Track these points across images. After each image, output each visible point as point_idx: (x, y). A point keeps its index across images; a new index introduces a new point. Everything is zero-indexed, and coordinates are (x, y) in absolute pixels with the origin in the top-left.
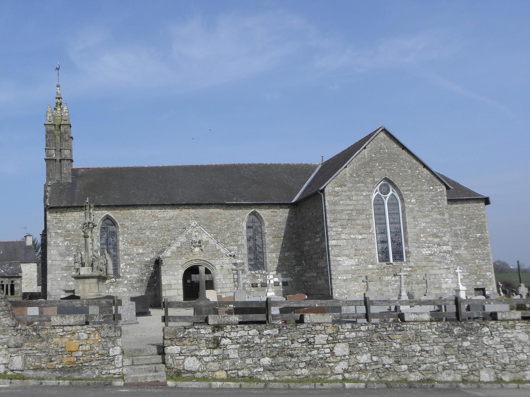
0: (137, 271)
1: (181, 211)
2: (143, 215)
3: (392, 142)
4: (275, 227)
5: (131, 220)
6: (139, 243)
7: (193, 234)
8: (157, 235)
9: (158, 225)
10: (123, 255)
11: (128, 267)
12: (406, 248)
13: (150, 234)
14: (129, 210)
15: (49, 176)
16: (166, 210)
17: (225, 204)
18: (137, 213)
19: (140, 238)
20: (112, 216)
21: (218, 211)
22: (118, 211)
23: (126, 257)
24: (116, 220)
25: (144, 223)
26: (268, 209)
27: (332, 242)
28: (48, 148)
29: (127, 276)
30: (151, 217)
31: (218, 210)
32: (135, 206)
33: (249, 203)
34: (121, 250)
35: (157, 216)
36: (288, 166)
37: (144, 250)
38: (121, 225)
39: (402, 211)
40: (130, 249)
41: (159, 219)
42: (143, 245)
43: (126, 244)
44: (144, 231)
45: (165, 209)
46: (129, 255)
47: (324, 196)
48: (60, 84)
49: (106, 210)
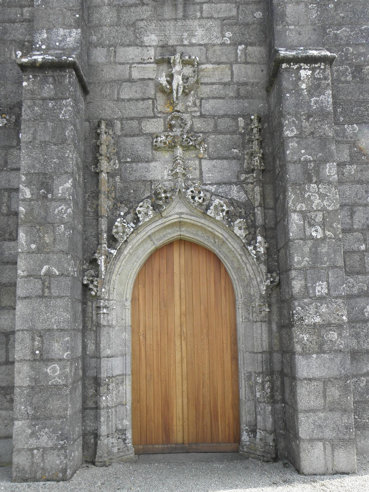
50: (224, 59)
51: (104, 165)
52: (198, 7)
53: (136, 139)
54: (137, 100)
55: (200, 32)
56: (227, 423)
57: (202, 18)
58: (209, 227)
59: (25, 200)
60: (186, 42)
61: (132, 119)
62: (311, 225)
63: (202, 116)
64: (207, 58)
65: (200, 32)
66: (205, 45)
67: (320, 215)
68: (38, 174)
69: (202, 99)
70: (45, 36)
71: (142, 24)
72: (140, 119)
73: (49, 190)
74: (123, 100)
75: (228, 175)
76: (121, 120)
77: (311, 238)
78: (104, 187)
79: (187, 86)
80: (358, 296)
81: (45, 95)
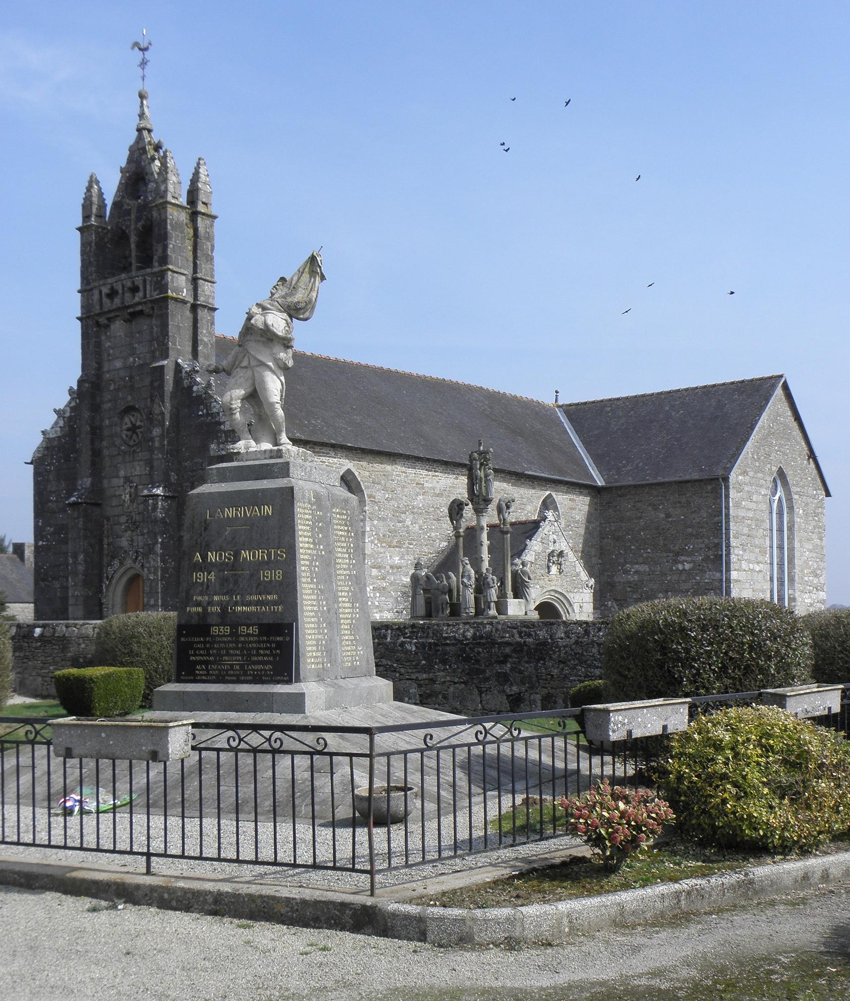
0: (390, 606)
1: (457, 478)
2: (402, 477)
3: (786, 404)
4: (572, 531)
5: (385, 489)
6: (395, 543)
7: (551, 538)
8: (421, 529)
9: (423, 506)
10: (371, 567)
11: (378, 595)
12: (791, 592)
13: (412, 524)
14: (382, 464)
15: (176, 345)
16: (437, 474)
17: (525, 475)
18: (394, 473)
19: (396, 531)
20: (356, 474)
21: (505, 487)
22: (364, 464)
23: (375, 572)
24: (362, 483)
25: (404, 498)
26: (566, 493)
27: (734, 575)
28: (175, 270)
29: (376, 614)
30: (414, 485)
31: (505, 485)
32: (392, 456)
33: (552, 477)
34: (368, 555)
35: (423, 484)
36: (495, 398)
37: (402, 558)
38: (370, 496)
39: (788, 527)
40: (381, 553)
41: (425, 492)
42: (400, 547)
43: (376, 542)
44: (403, 515)
45: (435, 471)
46: (379, 567)
47: (727, 488)
48: (148, 89)
49: (347, 457)
51: (106, 541)
55: (138, 468)
65: (138, 468)
71: (119, 465)
72: (118, 516)
73: (77, 560)
78: (106, 552)
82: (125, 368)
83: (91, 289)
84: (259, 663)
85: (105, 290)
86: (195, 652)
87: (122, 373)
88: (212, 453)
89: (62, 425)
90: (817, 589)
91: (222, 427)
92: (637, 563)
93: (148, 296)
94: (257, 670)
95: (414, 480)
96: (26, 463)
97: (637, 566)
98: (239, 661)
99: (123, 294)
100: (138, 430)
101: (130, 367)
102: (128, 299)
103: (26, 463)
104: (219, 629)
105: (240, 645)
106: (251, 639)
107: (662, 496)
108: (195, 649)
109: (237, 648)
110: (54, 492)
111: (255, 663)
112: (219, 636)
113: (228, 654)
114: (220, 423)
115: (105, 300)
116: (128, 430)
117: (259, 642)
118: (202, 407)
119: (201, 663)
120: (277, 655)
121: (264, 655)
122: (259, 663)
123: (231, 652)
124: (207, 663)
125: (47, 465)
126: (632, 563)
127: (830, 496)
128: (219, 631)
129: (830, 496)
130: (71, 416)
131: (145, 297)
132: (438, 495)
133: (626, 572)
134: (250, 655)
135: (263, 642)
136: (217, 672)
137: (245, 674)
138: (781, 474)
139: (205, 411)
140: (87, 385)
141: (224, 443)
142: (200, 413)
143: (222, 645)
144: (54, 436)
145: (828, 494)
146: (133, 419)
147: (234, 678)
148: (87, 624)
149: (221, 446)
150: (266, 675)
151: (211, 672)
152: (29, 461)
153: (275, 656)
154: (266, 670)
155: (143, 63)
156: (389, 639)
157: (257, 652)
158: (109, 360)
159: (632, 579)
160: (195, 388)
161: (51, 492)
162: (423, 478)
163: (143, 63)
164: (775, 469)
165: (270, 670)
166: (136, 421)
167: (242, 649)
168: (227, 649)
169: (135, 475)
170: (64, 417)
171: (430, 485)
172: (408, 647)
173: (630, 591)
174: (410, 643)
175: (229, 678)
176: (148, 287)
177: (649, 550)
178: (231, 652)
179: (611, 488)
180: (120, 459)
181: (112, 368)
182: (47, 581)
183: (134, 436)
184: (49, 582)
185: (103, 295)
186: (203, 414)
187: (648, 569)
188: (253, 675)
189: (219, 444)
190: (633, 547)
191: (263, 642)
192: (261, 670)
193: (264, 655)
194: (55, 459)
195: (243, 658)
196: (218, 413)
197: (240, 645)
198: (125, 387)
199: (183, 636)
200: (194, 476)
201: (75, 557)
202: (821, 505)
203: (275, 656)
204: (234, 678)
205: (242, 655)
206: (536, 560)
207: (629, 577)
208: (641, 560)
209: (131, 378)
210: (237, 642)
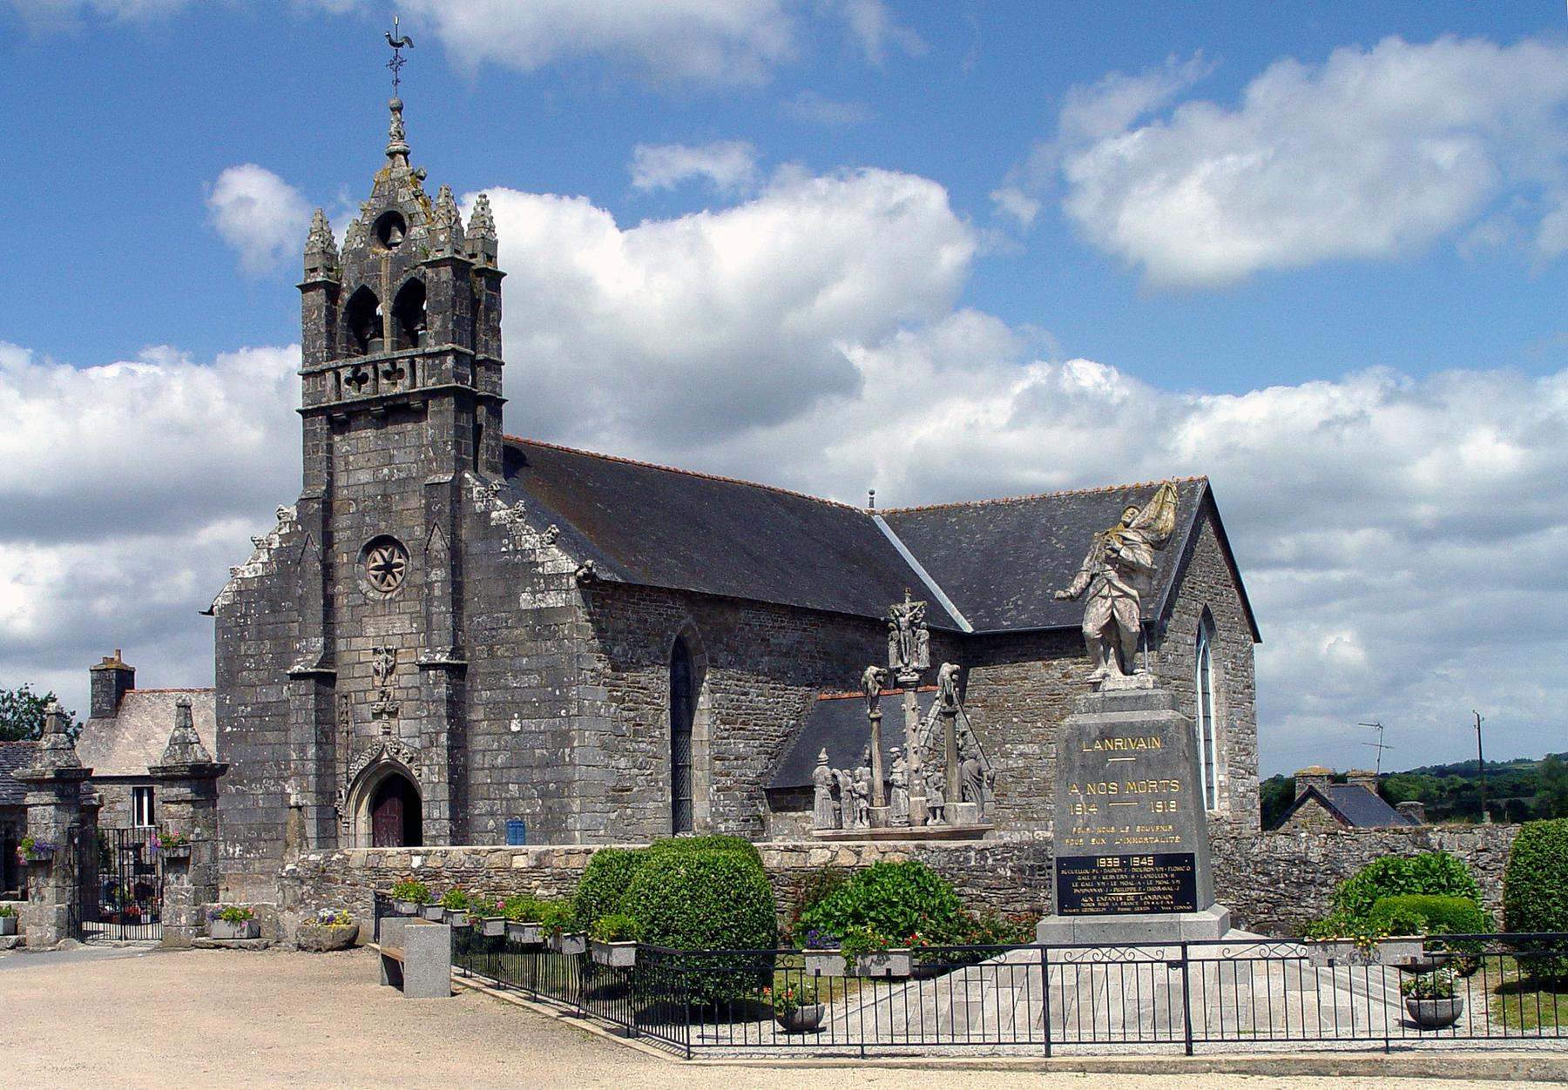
50: (412, 645)
52: (397, 605)
53: (363, 705)
54: (363, 677)
56: (604, 1033)
57: (399, 613)
58: (145, 855)
59: (293, 760)
60: (390, 633)
61: (361, 691)
62: (432, 774)
63: (400, 688)
64: (402, 644)
66: (401, 634)
67: (437, 767)
68: (299, 744)
69: (399, 675)
70: (305, 643)
73: (305, 755)
74: (356, 678)
75: (414, 731)
76: (354, 692)
77: (433, 782)
79: (85, 1017)
80: (484, 815)
81: (301, 693)
82: (376, 482)
83: (322, 372)
84: (1156, 893)
85: (346, 373)
86: (1079, 884)
87: (370, 490)
88: (523, 606)
89: (266, 561)
90: (1249, 773)
91: (540, 569)
92: (1022, 742)
93: (418, 385)
94: (1155, 901)
95: (759, 635)
96: (204, 613)
97: (1022, 747)
98: (1133, 892)
99: (376, 379)
100: (394, 570)
101: (384, 482)
102: (386, 388)
103: (204, 613)
104: (1107, 861)
105: (1133, 877)
106: (1146, 870)
107: (1056, 647)
108: (1080, 882)
109: (1130, 880)
110: (252, 656)
111: (1152, 893)
112: (1106, 867)
113: (1119, 886)
114: (537, 565)
115: (345, 387)
116: (378, 568)
117: (1155, 872)
118: (506, 541)
119: (1087, 895)
120: (1177, 885)
121: (1161, 886)
122: (1156, 893)
123: (1122, 883)
124: (1094, 895)
125: (240, 617)
126: (1013, 742)
127: (1260, 641)
128: (1107, 863)
129: (1260, 641)
130: (281, 547)
131: (414, 385)
132: (786, 655)
133: (1007, 755)
134: (1146, 886)
135: (1160, 872)
136: (1107, 904)
137: (1141, 905)
138: (1207, 615)
139: (511, 546)
140: (316, 506)
141: (543, 592)
142: (504, 549)
143: (1112, 877)
144: (253, 575)
145: (1257, 639)
146: (386, 554)
147: (1128, 909)
148: (500, 850)
149: (539, 596)
150: (1165, 905)
151: (1099, 904)
152: (206, 611)
153: (1174, 886)
154: (1165, 901)
155: (396, 63)
156: (973, 863)
157: (1154, 882)
158: (347, 470)
159: (1015, 765)
160: (494, 514)
161: (246, 655)
162: (768, 631)
163: (396, 63)
164: (1200, 607)
165: (1170, 900)
166: (392, 557)
167: (1135, 881)
168: (1118, 881)
169: (394, 634)
170: (269, 550)
171: (776, 641)
172: (1001, 871)
173: (1012, 782)
174: (1004, 867)
175: (1122, 910)
176: (419, 373)
177: (1039, 724)
178: (1122, 883)
179: (981, 636)
180: (367, 610)
181: (351, 482)
182: (241, 783)
183: (389, 577)
184: (244, 785)
185: (342, 380)
186: (508, 551)
187: (1038, 751)
188: (1150, 906)
189: (534, 593)
190: (1015, 720)
191: (1160, 872)
192: (1159, 900)
193: (1161, 886)
194: (254, 609)
195: (1137, 888)
196: (534, 551)
197: (1133, 877)
198: (375, 509)
199: (1064, 868)
200: (493, 637)
201: (302, 748)
202: (1251, 651)
203: (1174, 886)
204: (1128, 909)
205: (1137, 886)
206: (934, 744)
207: (1011, 762)
208: (1027, 737)
209: (385, 496)
210: (1129, 874)
